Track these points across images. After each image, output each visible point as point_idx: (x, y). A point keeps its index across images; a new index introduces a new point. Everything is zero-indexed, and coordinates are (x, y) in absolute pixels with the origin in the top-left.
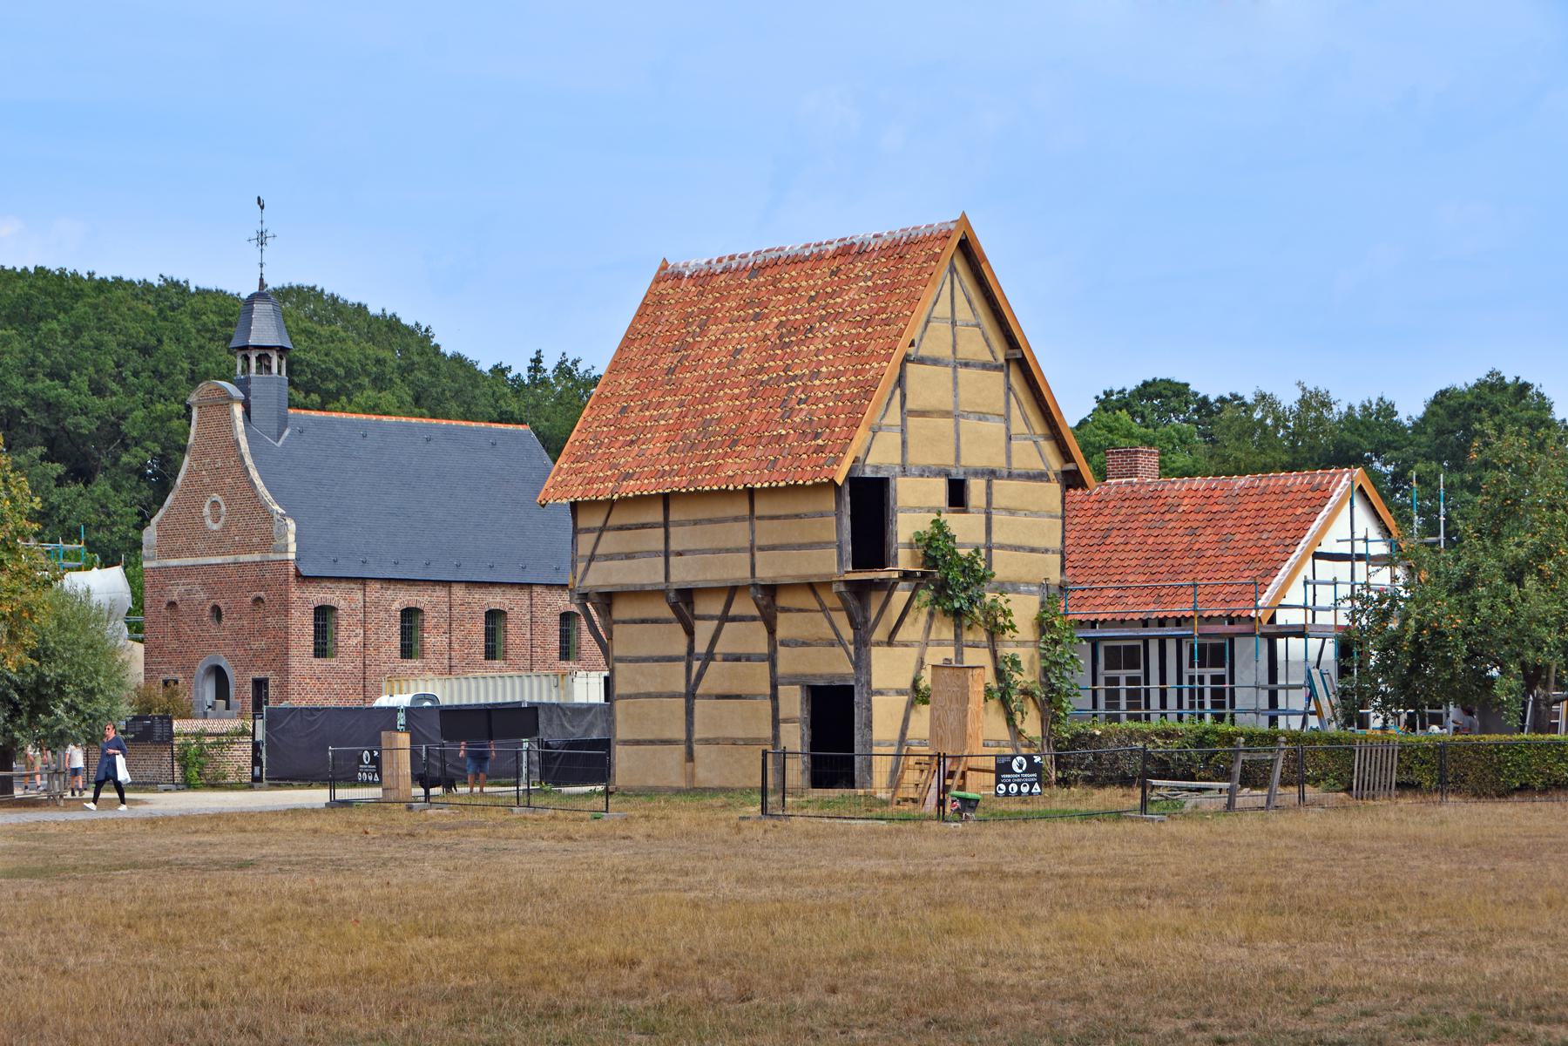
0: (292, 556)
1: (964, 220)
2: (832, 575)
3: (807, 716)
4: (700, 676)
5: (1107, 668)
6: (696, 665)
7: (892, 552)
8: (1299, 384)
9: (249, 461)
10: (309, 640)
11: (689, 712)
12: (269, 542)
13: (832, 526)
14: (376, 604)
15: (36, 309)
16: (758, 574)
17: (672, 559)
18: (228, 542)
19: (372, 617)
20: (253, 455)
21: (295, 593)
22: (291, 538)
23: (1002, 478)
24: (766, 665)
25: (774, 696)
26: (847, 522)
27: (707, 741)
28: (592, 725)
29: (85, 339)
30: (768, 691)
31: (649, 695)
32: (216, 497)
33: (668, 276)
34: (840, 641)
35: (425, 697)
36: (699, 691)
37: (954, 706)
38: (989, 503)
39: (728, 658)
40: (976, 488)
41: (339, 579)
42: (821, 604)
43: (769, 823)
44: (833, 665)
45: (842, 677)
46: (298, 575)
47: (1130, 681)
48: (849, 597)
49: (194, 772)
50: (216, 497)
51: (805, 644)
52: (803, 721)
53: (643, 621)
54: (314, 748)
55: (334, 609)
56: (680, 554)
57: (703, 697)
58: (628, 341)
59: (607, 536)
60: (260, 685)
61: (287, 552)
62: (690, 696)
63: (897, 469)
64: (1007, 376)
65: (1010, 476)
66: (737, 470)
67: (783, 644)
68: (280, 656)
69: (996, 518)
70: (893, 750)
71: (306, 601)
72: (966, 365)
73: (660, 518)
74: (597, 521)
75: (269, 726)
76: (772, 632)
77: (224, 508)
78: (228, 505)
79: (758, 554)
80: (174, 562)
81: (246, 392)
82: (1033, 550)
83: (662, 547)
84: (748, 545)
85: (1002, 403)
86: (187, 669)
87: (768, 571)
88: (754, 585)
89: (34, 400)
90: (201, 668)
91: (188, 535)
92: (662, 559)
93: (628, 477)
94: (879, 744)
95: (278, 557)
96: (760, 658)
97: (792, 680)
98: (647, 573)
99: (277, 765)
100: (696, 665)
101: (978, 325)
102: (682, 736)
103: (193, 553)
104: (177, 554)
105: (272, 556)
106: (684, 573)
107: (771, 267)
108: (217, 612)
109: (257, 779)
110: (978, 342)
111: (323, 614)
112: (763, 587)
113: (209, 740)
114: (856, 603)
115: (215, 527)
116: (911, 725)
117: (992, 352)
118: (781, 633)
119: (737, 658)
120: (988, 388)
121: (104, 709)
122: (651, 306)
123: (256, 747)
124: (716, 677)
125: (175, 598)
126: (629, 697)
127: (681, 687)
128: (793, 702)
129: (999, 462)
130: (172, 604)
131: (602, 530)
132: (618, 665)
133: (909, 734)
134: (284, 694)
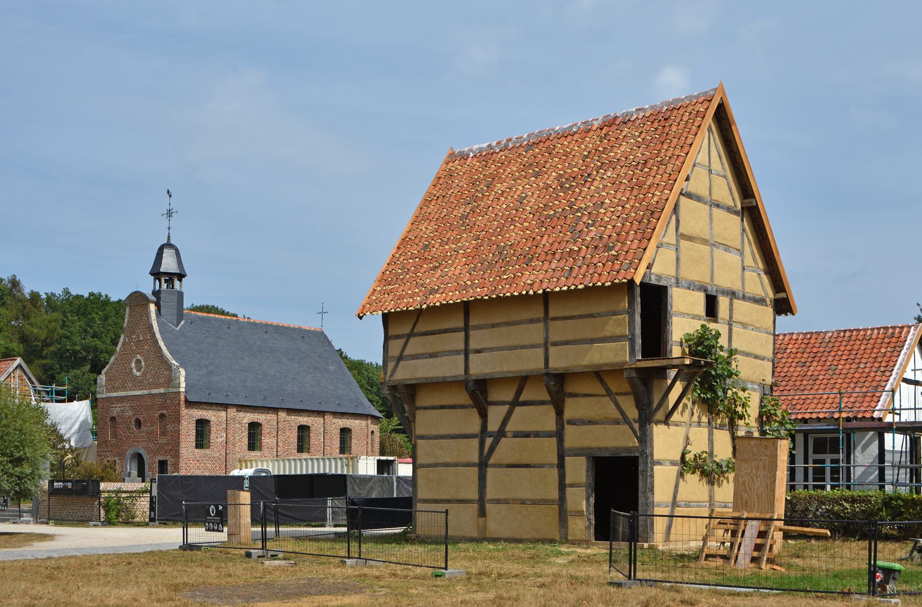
0: (182, 390)
1: (721, 88)
2: (625, 363)
3: (593, 485)
4: (492, 449)
5: (814, 453)
6: (489, 441)
7: (668, 348)
9: (158, 336)
10: (193, 438)
11: (482, 478)
12: (171, 380)
13: (626, 322)
14: (234, 419)
15: (89, 309)
16: (551, 365)
17: (472, 357)
18: (145, 382)
19: (231, 427)
20: (161, 333)
21: (184, 411)
22: (182, 379)
23: (738, 299)
24: (554, 441)
25: (561, 465)
26: (638, 319)
27: (498, 501)
28: (372, 489)
29: (110, 321)
30: (555, 461)
31: (447, 465)
32: (139, 357)
34: (626, 420)
35: (262, 471)
36: (492, 461)
37: (761, 473)
38: (731, 317)
39: (517, 435)
40: (723, 303)
41: (211, 404)
42: (607, 389)
44: (617, 439)
45: (628, 449)
46: (186, 401)
47: (833, 461)
48: (638, 382)
49: (113, 515)
50: (139, 357)
51: (591, 422)
52: (587, 486)
53: (442, 407)
54: (189, 500)
55: (208, 422)
56: (478, 351)
57: (494, 466)
58: (426, 202)
59: (413, 341)
60: (163, 465)
62: (483, 465)
63: (673, 281)
64: (742, 221)
65: (744, 298)
66: (534, 279)
67: (570, 422)
68: (175, 448)
69: (734, 329)
72: (718, 206)
73: (461, 324)
74: (406, 330)
75: (159, 488)
76: (560, 413)
78: (146, 361)
79: (552, 350)
80: (115, 394)
81: (159, 298)
82: (756, 357)
83: (462, 347)
84: (542, 341)
85: (739, 241)
86: (122, 455)
87: (560, 360)
88: (547, 374)
89: (87, 349)
90: (130, 452)
91: (123, 378)
92: (462, 357)
93: (433, 292)
94: (658, 506)
95: (174, 390)
96: (549, 435)
97: (578, 452)
98: (451, 368)
99: (163, 514)
100: (489, 441)
101: (725, 177)
102: (475, 496)
103: (124, 388)
104: (116, 389)
105: (171, 390)
106: (480, 367)
107: (545, 143)
108: (138, 423)
109: (152, 520)
110: (725, 190)
111: (202, 426)
112: (556, 375)
113: (124, 495)
114: (643, 388)
115: (138, 374)
116: (680, 490)
117: (734, 200)
118: (568, 414)
119: (527, 435)
120: (733, 227)
121: (29, 471)
122: (444, 179)
123: (151, 498)
124: (506, 450)
125: (115, 415)
126: (429, 466)
127: (475, 459)
128: (578, 470)
129: (737, 286)
130: (113, 419)
131: (409, 336)
132: (419, 442)
133: (679, 498)
134: (176, 467)
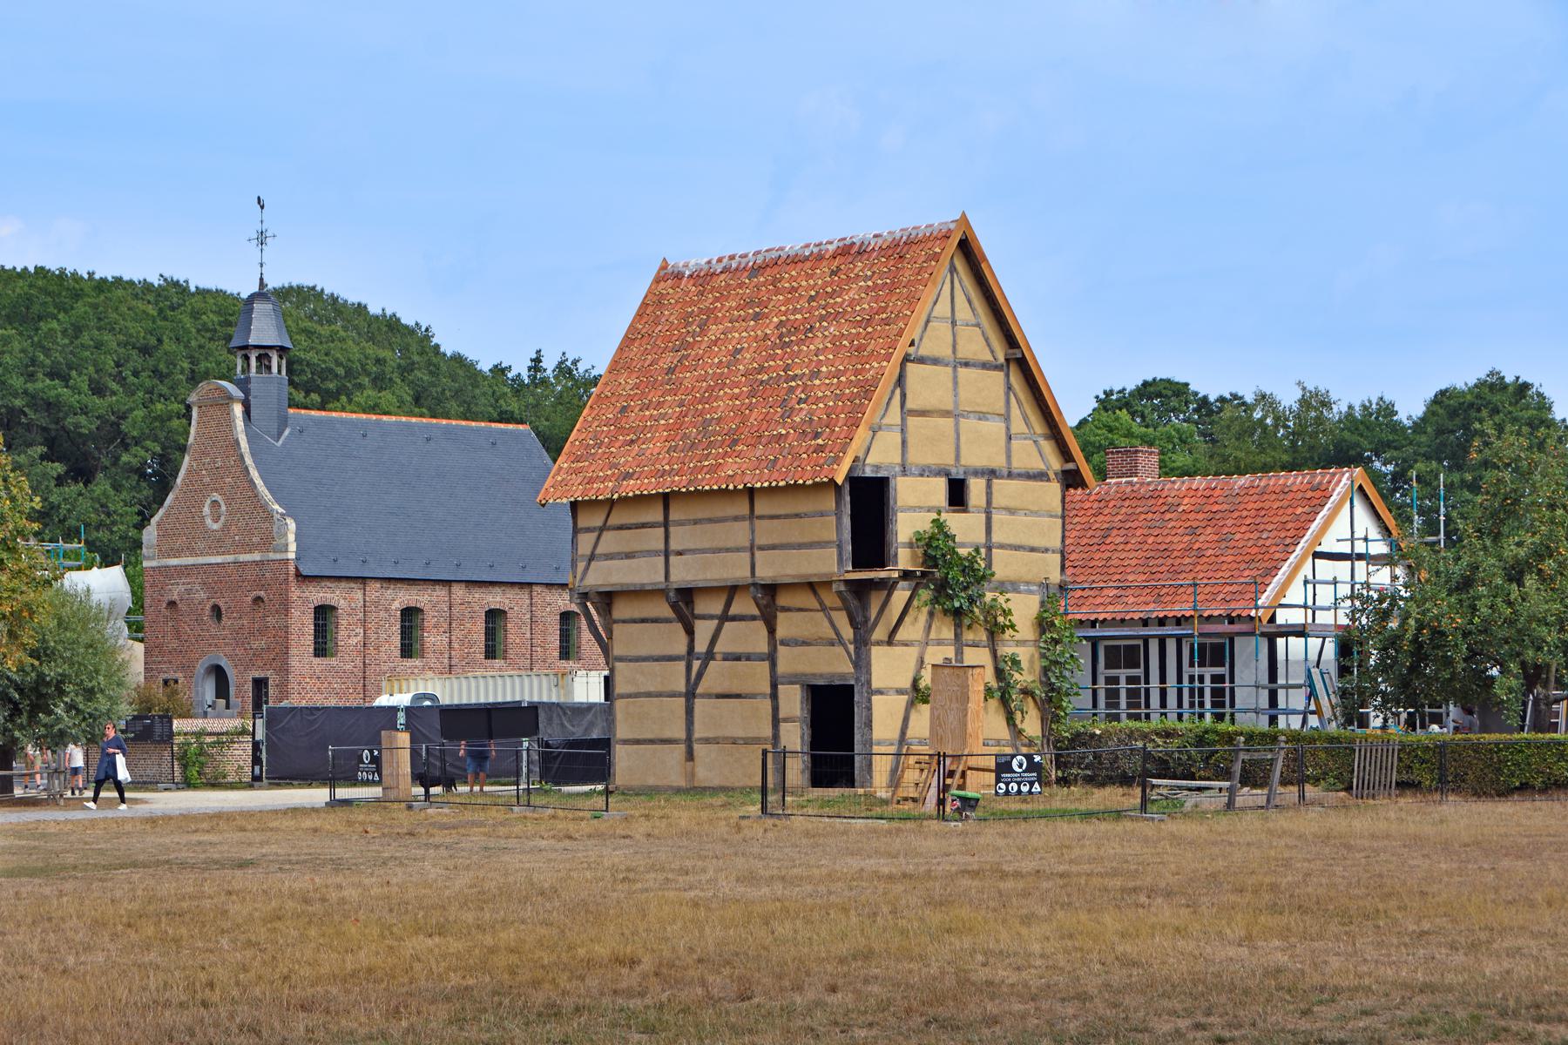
0: (292, 556)
1: (964, 220)
2: (832, 574)
3: (807, 715)
4: (700, 675)
5: (1107, 667)
6: (696, 664)
7: (892, 552)
8: (1299, 383)
9: (249, 461)
10: (309, 639)
11: (689, 712)
12: (269, 541)
13: (832, 526)
14: (376, 603)
15: (36, 308)
16: (758, 574)
17: (672, 559)
18: (228, 541)
19: (372, 617)
20: (253, 455)
21: (295, 592)
22: (291, 537)
23: (1002, 477)
24: (766, 664)
25: (774, 696)
26: (847, 521)
27: (707, 741)
28: (592, 724)
29: (85, 338)
30: (768, 690)
31: (649, 695)
32: (216, 496)
33: (668, 276)
34: (840, 641)
35: (425, 696)
36: (699, 690)
37: (954, 706)
38: (989, 502)
39: (728, 657)
40: (976, 488)
41: (339, 578)
42: (821, 603)
43: (769, 822)
44: (833, 665)
45: (842, 676)
46: (298, 575)
47: (1130, 680)
48: (849, 596)
49: (194, 771)
50: (216, 496)
51: (805, 643)
52: (803, 721)
53: (643, 621)
54: (314, 748)
55: (334, 608)
56: (680, 553)
57: (703, 696)
58: (628, 341)
59: (607, 536)
60: (260, 685)
61: (287, 551)
62: (690, 695)
63: (897, 469)
64: (1007, 375)
65: (1010, 475)
66: (737, 469)
67: (783, 643)
68: (280, 656)
69: (996, 517)
70: (893, 749)
71: (306, 601)
72: (966, 364)
73: (660, 518)
74: (597, 521)
75: (269, 725)
76: (772, 631)
77: (224, 508)
78: (228, 505)
79: (758, 554)
80: (174, 562)
81: (246, 392)
82: (1033, 550)
83: (662, 546)
84: (748, 544)
85: (1002, 403)
86: (187, 668)
87: (768, 570)
88: (754, 585)
89: (34, 400)
90: (201, 667)
91: (188, 535)
92: (662, 559)
93: (628, 476)
94: (879, 744)
95: (278, 556)
96: (760, 657)
97: (792, 679)
98: (647, 573)
99: (277, 765)
100: (696, 664)
101: (978, 325)
102: (682, 735)
103: (193, 552)
104: (177, 553)
105: (272, 556)
106: (684, 573)
107: (771, 267)
108: (217, 612)
109: (257, 778)
110: (978, 341)
111: (323, 614)
112: (763, 586)
113: (209, 740)
114: (856, 602)
115: (215, 526)
116: (911, 724)
117: (992, 352)
118: (781, 632)
119: (737, 658)
120: (988, 388)
121: (104, 708)
122: (651, 306)
123: (256, 746)
124: (716, 676)
125: (175, 597)
126: (629, 696)
127: (681, 687)
128: (793, 701)
129: (999, 462)
130: (172, 604)
131: (602, 529)
132: (618, 665)
133: (909, 733)
134: (284, 693)
